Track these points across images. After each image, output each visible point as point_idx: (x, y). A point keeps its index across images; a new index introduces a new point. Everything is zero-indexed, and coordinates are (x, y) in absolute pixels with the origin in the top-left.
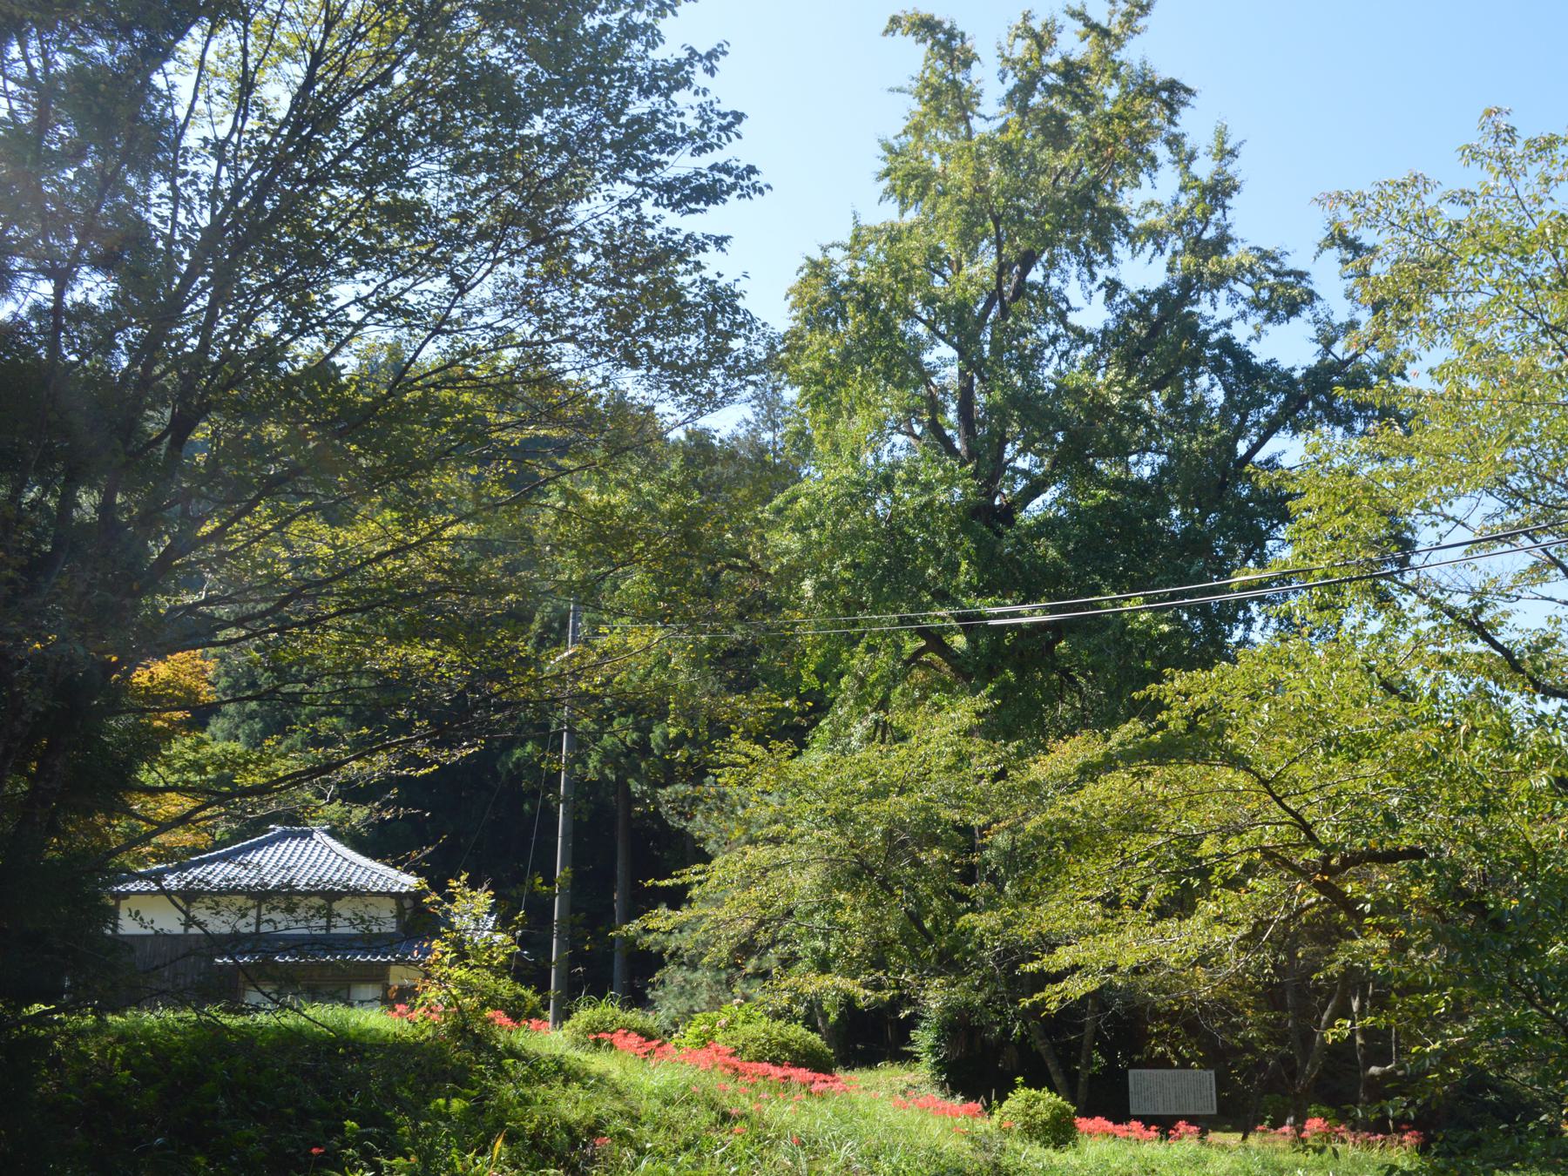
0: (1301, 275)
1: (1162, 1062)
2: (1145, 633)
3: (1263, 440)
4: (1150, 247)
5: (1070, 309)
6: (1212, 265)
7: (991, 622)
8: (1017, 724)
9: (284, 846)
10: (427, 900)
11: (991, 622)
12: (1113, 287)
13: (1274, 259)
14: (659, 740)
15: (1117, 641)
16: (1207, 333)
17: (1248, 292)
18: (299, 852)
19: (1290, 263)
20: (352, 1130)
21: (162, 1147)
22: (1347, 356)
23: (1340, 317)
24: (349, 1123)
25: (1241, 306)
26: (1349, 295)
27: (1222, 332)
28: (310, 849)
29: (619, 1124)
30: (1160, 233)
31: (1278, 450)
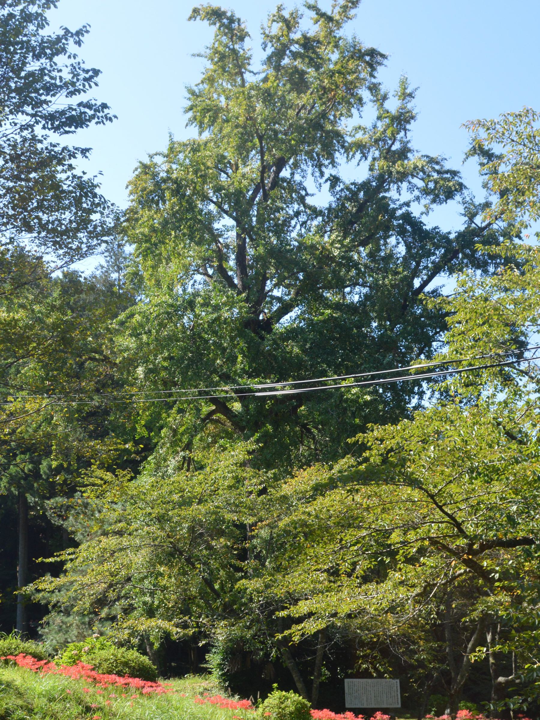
0: (454, 173)
2: (355, 401)
5: (307, 194)
6: (398, 167)
12: (335, 181)
13: (437, 163)
14: (46, 469)
15: (337, 406)
16: (394, 210)
17: (420, 184)
19: (448, 166)
22: (484, 225)
23: (480, 200)
27: (404, 210)
30: (365, 146)
31: (440, 284)
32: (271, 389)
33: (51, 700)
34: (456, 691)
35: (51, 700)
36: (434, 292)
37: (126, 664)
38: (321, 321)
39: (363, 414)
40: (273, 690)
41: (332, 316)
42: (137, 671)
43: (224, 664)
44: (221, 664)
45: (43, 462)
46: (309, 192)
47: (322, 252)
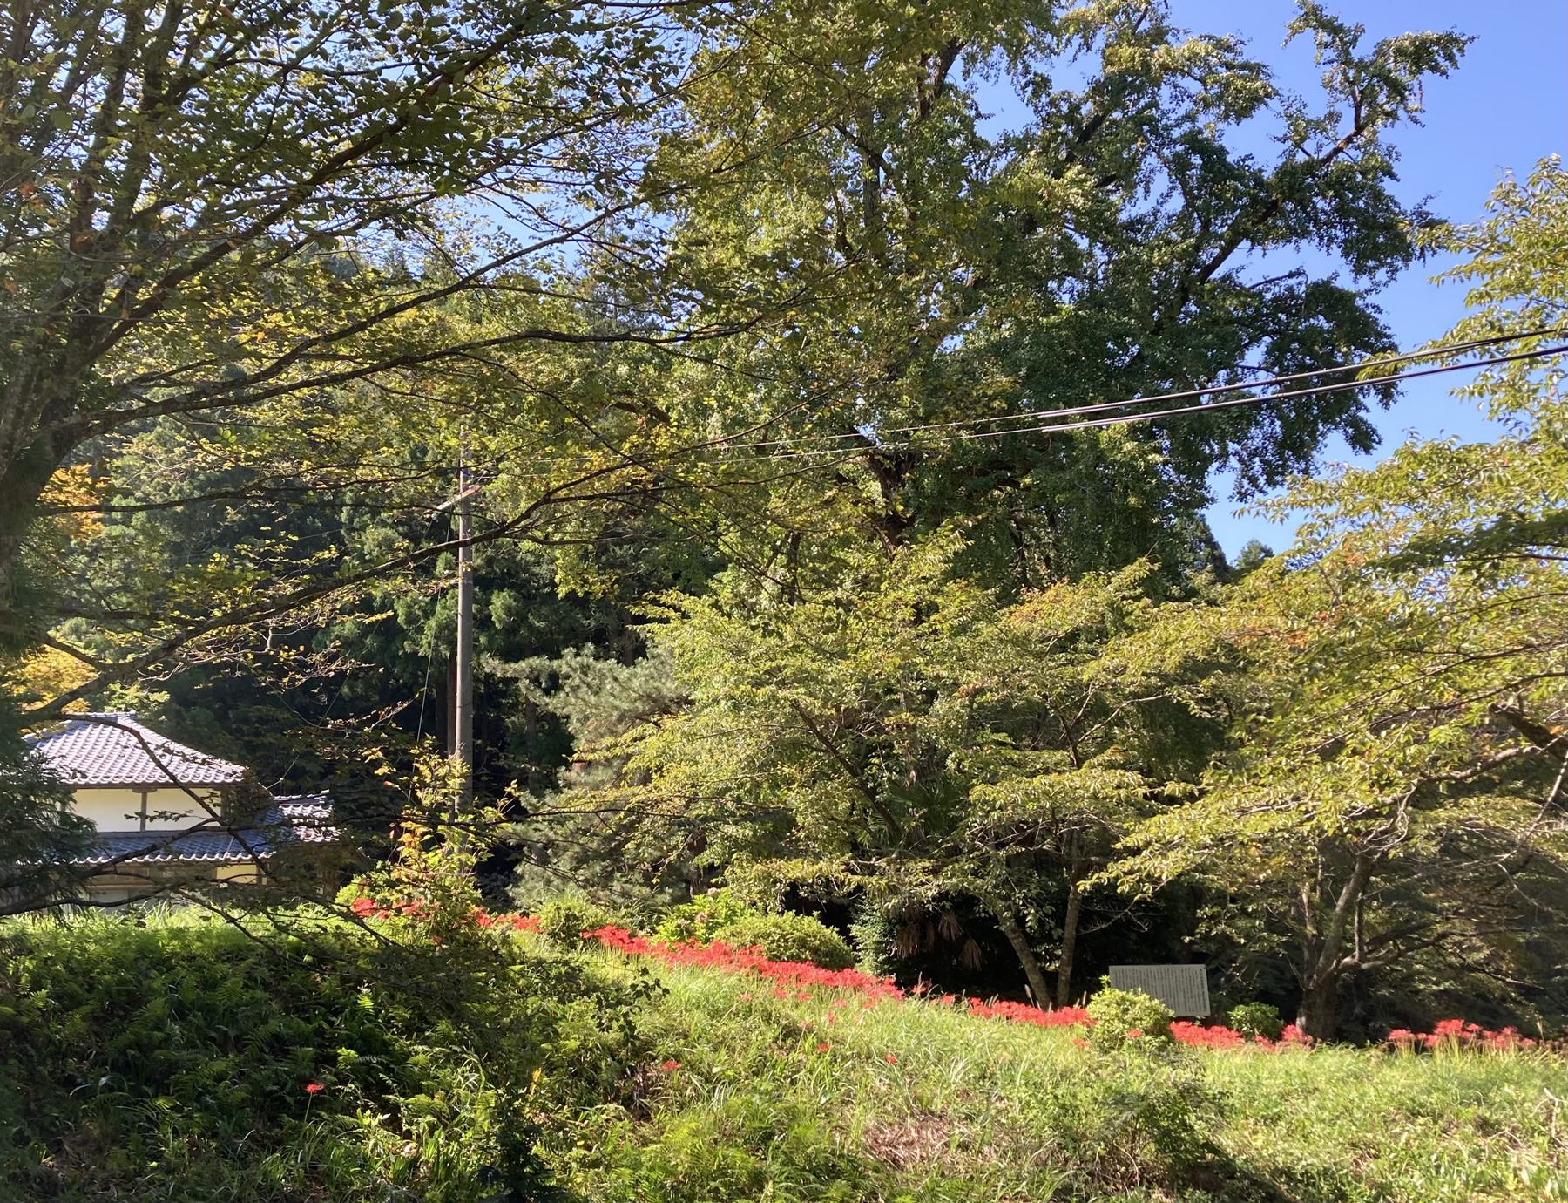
0: (1256, 69)
1: (1027, 1002)
2: (1130, 466)
3: (1225, 253)
4: (1077, 40)
5: (979, 116)
6: (1160, 54)
7: (1046, 429)
8: (997, 568)
9: (86, 733)
10: (379, 772)
11: (1046, 429)
12: (1042, 84)
13: (1229, 49)
14: (500, 612)
15: (1091, 476)
16: (1167, 128)
17: (1195, 87)
18: (92, 740)
19: (1249, 54)
20: (347, 1058)
21: (108, 1088)
22: (1322, 155)
23: (1316, 111)
24: (343, 1051)
25: (1187, 105)
26: (1328, 85)
27: (1187, 126)
28: (94, 737)
29: (668, 1045)
30: (1087, 24)
31: (1237, 266)
32: (1063, 420)
33: (715, 1014)
34: (1317, 985)
35: (715, 1014)
36: (1224, 279)
37: (802, 943)
38: (1053, 325)
39: (1147, 487)
40: (1101, 987)
41: (1077, 316)
42: (826, 955)
43: (888, 943)
44: (880, 942)
45: (494, 599)
46: (982, 110)
47: (1047, 203)
